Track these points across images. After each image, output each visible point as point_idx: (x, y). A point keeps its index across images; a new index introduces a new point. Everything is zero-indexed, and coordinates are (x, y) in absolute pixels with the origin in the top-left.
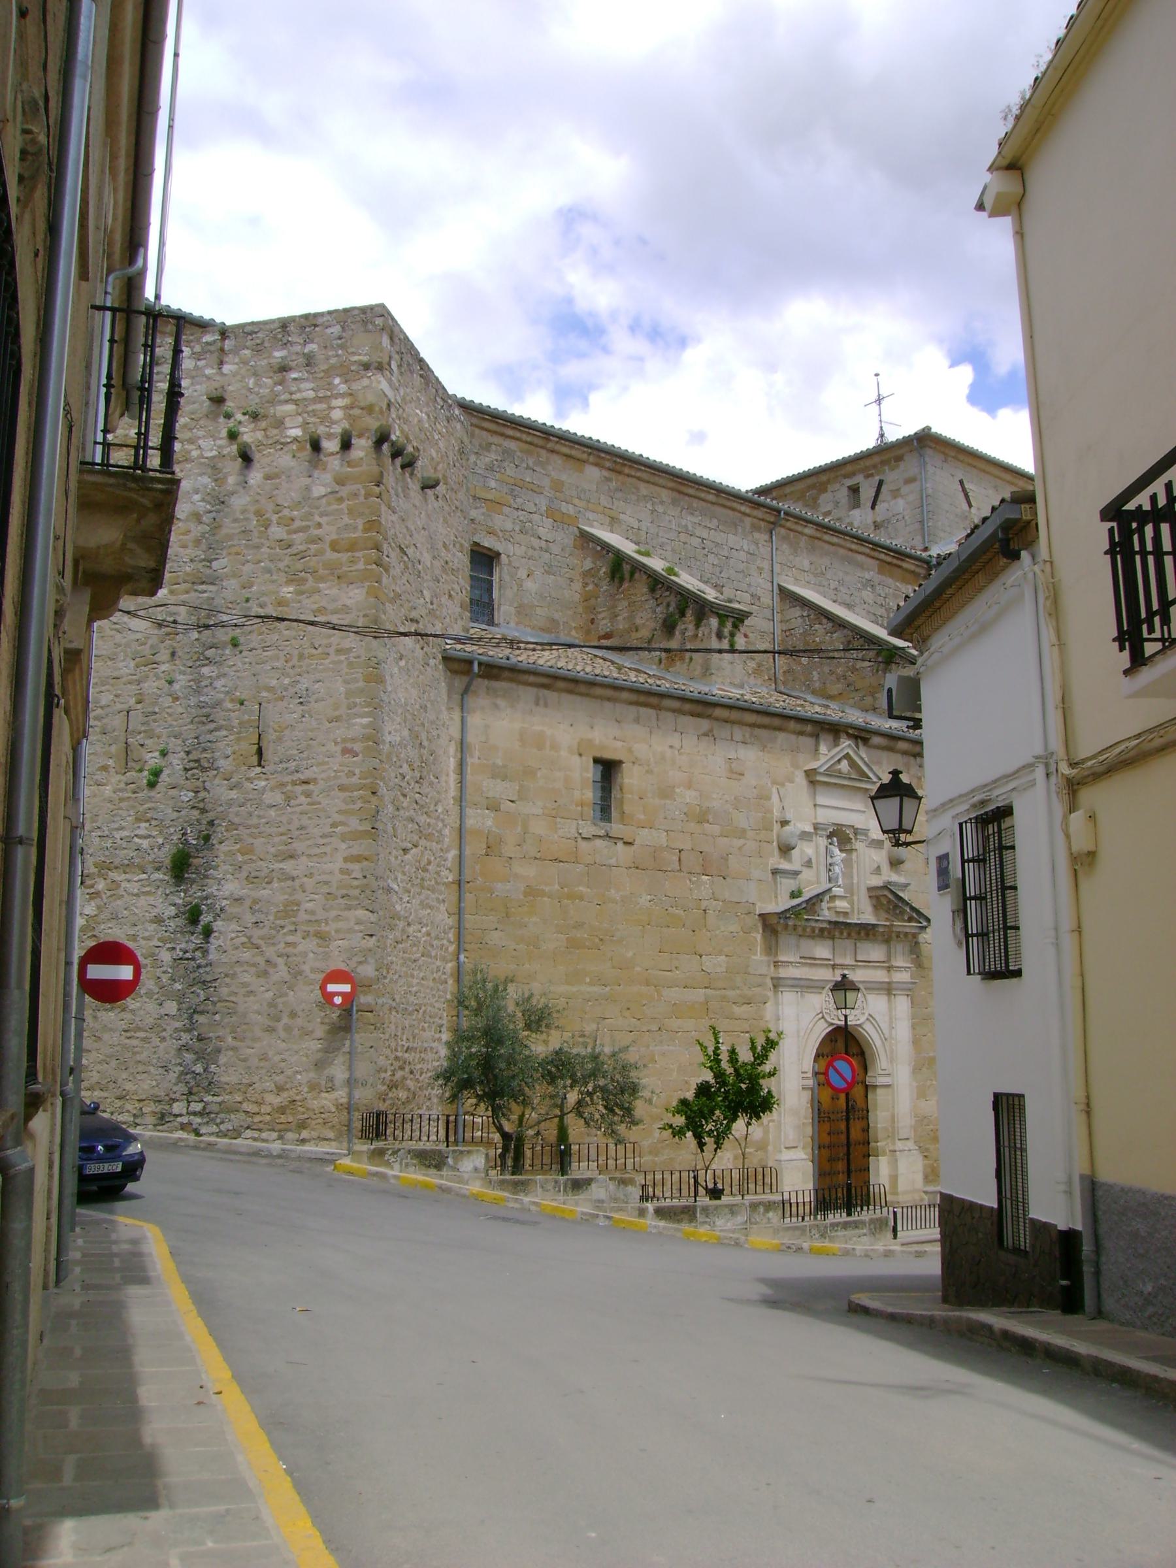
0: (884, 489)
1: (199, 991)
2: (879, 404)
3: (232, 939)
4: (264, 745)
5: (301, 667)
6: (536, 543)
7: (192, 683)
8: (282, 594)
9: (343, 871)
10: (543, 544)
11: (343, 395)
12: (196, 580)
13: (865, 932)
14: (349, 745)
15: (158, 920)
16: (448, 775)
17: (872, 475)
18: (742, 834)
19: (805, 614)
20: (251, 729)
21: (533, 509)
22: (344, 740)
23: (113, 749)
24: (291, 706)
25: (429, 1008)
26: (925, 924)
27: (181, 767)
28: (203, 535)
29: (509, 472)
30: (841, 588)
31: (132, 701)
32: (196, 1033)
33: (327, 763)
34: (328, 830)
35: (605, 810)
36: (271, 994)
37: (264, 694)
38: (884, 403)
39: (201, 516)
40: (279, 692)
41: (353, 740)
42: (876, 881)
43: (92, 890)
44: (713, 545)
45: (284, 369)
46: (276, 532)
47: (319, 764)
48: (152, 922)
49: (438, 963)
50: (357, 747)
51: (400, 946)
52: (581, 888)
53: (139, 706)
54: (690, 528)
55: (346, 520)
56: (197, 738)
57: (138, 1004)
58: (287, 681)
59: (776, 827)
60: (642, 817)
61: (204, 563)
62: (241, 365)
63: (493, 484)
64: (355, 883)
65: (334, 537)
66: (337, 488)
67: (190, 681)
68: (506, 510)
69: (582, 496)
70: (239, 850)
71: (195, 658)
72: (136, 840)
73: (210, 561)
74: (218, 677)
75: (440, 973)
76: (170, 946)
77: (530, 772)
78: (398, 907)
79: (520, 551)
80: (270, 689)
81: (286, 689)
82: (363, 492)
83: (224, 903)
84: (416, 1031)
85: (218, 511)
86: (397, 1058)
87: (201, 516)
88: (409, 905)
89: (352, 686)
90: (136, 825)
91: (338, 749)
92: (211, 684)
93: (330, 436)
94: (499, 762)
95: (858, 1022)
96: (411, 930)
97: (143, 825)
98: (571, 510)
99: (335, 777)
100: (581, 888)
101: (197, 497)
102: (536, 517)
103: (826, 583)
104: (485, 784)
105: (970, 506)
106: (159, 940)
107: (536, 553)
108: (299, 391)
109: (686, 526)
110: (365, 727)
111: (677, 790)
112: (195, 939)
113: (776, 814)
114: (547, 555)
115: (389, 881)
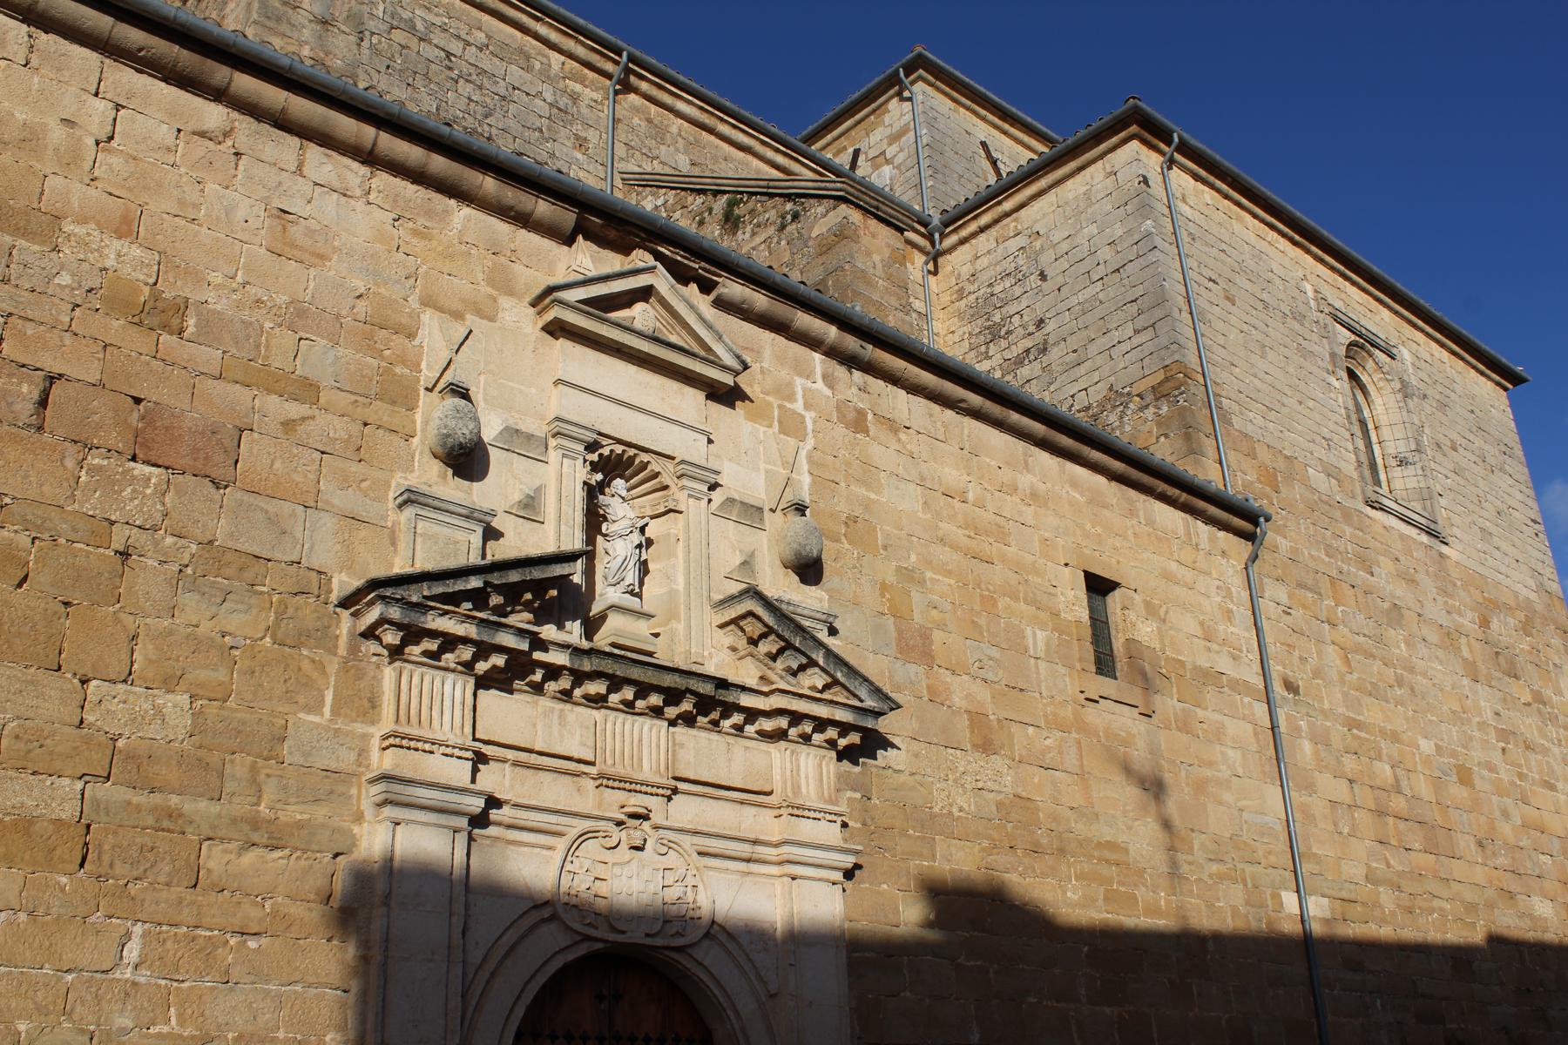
17: (845, 148)
26: (870, 703)
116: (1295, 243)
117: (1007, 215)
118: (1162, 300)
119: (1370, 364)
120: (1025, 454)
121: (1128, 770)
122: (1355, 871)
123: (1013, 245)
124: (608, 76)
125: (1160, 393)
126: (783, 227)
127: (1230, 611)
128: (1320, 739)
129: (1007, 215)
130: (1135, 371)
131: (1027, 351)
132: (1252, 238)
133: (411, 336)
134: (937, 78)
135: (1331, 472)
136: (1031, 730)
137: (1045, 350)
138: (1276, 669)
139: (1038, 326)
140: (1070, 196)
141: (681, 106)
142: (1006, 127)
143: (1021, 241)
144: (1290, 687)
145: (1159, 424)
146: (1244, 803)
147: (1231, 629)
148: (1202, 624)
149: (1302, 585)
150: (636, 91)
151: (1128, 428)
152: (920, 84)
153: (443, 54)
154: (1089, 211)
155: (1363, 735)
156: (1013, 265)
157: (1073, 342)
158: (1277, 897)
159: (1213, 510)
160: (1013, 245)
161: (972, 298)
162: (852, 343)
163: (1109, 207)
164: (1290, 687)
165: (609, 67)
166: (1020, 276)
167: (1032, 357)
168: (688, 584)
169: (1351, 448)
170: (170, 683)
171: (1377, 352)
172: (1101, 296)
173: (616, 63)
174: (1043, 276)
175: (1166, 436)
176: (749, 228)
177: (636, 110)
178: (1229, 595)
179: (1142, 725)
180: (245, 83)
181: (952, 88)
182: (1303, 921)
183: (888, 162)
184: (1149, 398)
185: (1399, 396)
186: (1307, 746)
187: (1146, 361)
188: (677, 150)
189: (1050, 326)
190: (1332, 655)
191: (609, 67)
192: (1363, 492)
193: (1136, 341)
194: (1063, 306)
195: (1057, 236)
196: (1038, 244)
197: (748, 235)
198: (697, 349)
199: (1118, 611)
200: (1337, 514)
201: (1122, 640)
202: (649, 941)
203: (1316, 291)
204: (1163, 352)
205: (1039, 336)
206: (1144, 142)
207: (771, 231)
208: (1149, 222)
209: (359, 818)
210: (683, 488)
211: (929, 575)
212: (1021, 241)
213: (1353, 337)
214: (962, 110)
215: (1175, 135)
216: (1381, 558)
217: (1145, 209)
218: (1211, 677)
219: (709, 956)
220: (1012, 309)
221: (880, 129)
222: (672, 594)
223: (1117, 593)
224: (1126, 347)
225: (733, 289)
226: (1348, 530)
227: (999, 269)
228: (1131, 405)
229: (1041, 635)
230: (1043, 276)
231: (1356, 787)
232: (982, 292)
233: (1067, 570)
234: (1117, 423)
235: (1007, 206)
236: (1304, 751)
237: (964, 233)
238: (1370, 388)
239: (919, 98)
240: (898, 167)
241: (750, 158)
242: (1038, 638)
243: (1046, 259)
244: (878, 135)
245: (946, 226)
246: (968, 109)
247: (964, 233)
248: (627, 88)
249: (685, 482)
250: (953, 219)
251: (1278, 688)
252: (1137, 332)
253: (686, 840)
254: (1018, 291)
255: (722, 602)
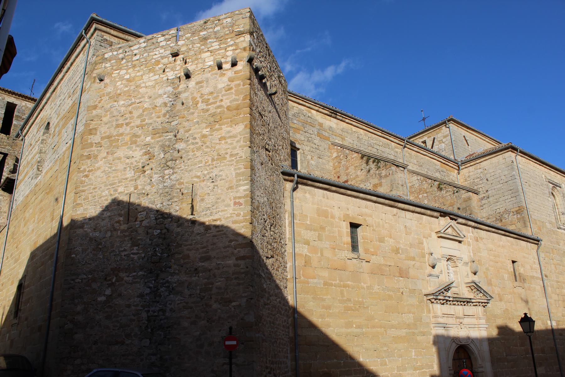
0: (435, 140)
1: (161, 333)
2: (424, 121)
3: (178, 304)
4: (194, 204)
5: (213, 165)
6: (314, 146)
7: (160, 178)
8: (204, 133)
9: (235, 265)
10: (317, 147)
11: (232, 45)
12: (163, 132)
13: (467, 302)
14: (237, 201)
15: (141, 296)
16: (285, 227)
17: (431, 137)
18: (413, 259)
19: (419, 178)
20: (188, 197)
21: (312, 133)
22: (235, 198)
23: (123, 212)
24: (208, 184)
25: (282, 341)
26: (489, 298)
27: (154, 218)
28: (167, 112)
29: (301, 118)
30: (429, 172)
31: (132, 189)
32: (159, 356)
33: (226, 210)
34: (227, 244)
35: (354, 247)
36: (198, 333)
37: (195, 179)
38: (426, 120)
39: (167, 104)
40: (202, 178)
41: (240, 198)
42: (469, 280)
43: (110, 282)
44: (381, 152)
45: (205, 39)
46: (201, 106)
47: (222, 211)
48: (138, 297)
49: (285, 318)
50: (242, 201)
51: (267, 306)
52: (348, 282)
53: (136, 191)
54: (372, 145)
55: (234, 97)
56: (162, 204)
57: (130, 341)
58: (206, 172)
59: (427, 256)
60: (372, 250)
61: (167, 124)
62: (186, 40)
63: (295, 122)
64: (243, 271)
65: (229, 104)
66: (229, 83)
67: (159, 177)
68: (301, 132)
69: (331, 129)
70: (181, 258)
71: (162, 166)
72: (132, 256)
73: (170, 123)
74: (173, 174)
75: (286, 323)
76: (146, 309)
77: (323, 228)
78: (265, 286)
79: (308, 148)
80: (198, 177)
81: (205, 176)
82: (242, 83)
83: (175, 285)
84: (276, 353)
85: (175, 101)
86: (267, 368)
87: (167, 104)
88: (270, 286)
89: (238, 171)
90: (132, 248)
91: (232, 202)
92: (169, 177)
93: (226, 62)
94: (308, 222)
95: (468, 343)
96: (271, 298)
97: (135, 248)
98: (327, 134)
99: (231, 217)
100: (348, 282)
101: (165, 96)
102: (313, 136)
103: (423, 169)
104: (302, 232)
105: (468, 145)
106: (142, 306)
107: (314, 150)
108: (212, 46)
109: (371, 144)
110: (245, 190)
111: (386, 239)
112: (159, 305)
113: (426, 251)
114: (318, 151)
115: (260, 271)
116: (540, 165)
117: (478, 163)
118: (517, 191)
119: (556, 190)
120: (501, 238)
121: (522, 299)
122: (560, 314)
123: (479, 171)
124: (402, 146)
125: (518, 212)
126: (454, 193)
127: (535, 262)
128: (552, 286)
129: (478, 163)
130: (511, 206)
131: (484, 197)
132: (532, 167)
133: (423, 244)
134: (454, 122)
135: (551, 223)
136: (507, 295)
137: (489, 197)
138: (543, 272)
139: (486, 192)
140: (494, 162)
141: (414, 149)
142: (468, 130)
143: (481, 170)
144: (546, 276)
145: (518, 219)
146: (540, 303)
147: (535, 266)
148: (530, 266)
149: (547, 252)
150: (406, 147)
151: (510, 219)
152: (451, 124)
153: (376, 150)
154: (499, 166)
155: (560, 284)
156: (479, 176)
157: (496, 197)
158: (547, 322)
159: (531, 241)
160: (479, 171)
161: (469, 182)
162: (476, 225)
163: (504, 167)
164: (546, 276)
165: (402, 144)
166: (481, 179)
167: (485, 199)
168: (461, 280)
169: (554, 215)
170: (410, 313)
171: (558, 188)
172: (502, 187)
173: (404, 143)
174: (487, 180)
175: (519, 222)
176: (445, 191)
177: (407, 152)
178: (534, 258)
179: (523, 290)
180: (400, 205)
181: (458, 124)
182: (551, 327)
183: (443, 143)
184: (515, 213)
185: (562, 198)
186: (550, 288)
187: (514, 205)
188: (414, 159)
189: (489, 192)
190: (553, 266)
191: (402, 144)
192: (557, 225)
193: (512, 199)
194: (493, 188)
195: (491, 171)
196: (486, 172)
197: (444, 193)
198: (458, 236)
199: (517, 267)
200: (552, 233)
201: (518, 273)
202: (465, 344)
203: (545, 176)
204: (518, 203)
205: (487, 194)
206: (512, 152)
207: (451, 193)
208: (514, 172)
209: (431, 329)
210: (458, 262)
211: (490, 268)
212: (481, 170)
213: (553, 185)
214: (459, 128)
215: (519, 150)
216: (561, 241)
217: (513, 169)
218: (533, 277)
219: (472, 345)
220: (480, 186)
221: (440, 134)
222: (458, 282)
223: (516, 263)
224: (509, 200)
225: (460, 220)
226: (554, 236)
227: (476, 176)
228: (511, 214)
229: (506, 275)
230: (487, 180)
231: (559, 296)
232: (471, 181)
233: (509, 261)
234: (507, 218)
235: (478, 162)
236: (549, 290)
237: (466, 166)
238: (556, 196)
239: (451, 128)
240: (446, 144)
241: (426, 157)
242: (506, 276)
243: (488, 176)
244: (440, 135)
245: (462, 164)
246: (460, 128)
247: (466, 166)
248: (405, 147)
249: (459, 261)
250: (464, 163)
251: (544, 277)
252: (512, 197)
253: (467, 326)
254: (481, 182)
255: (467, 283)
